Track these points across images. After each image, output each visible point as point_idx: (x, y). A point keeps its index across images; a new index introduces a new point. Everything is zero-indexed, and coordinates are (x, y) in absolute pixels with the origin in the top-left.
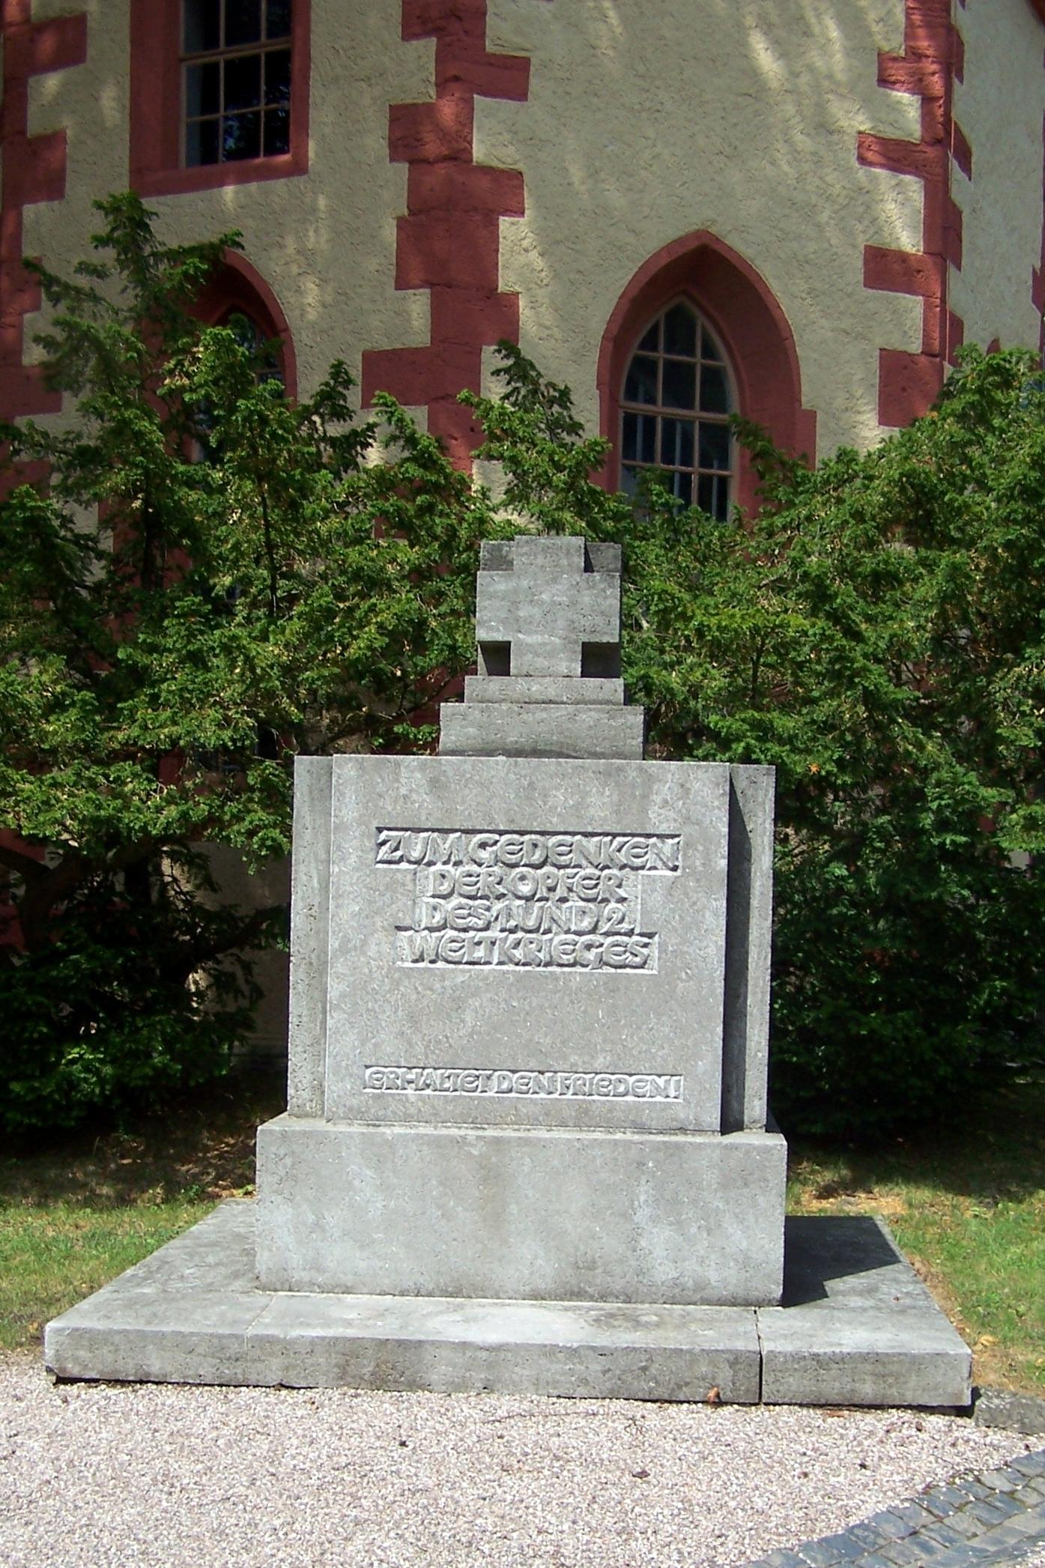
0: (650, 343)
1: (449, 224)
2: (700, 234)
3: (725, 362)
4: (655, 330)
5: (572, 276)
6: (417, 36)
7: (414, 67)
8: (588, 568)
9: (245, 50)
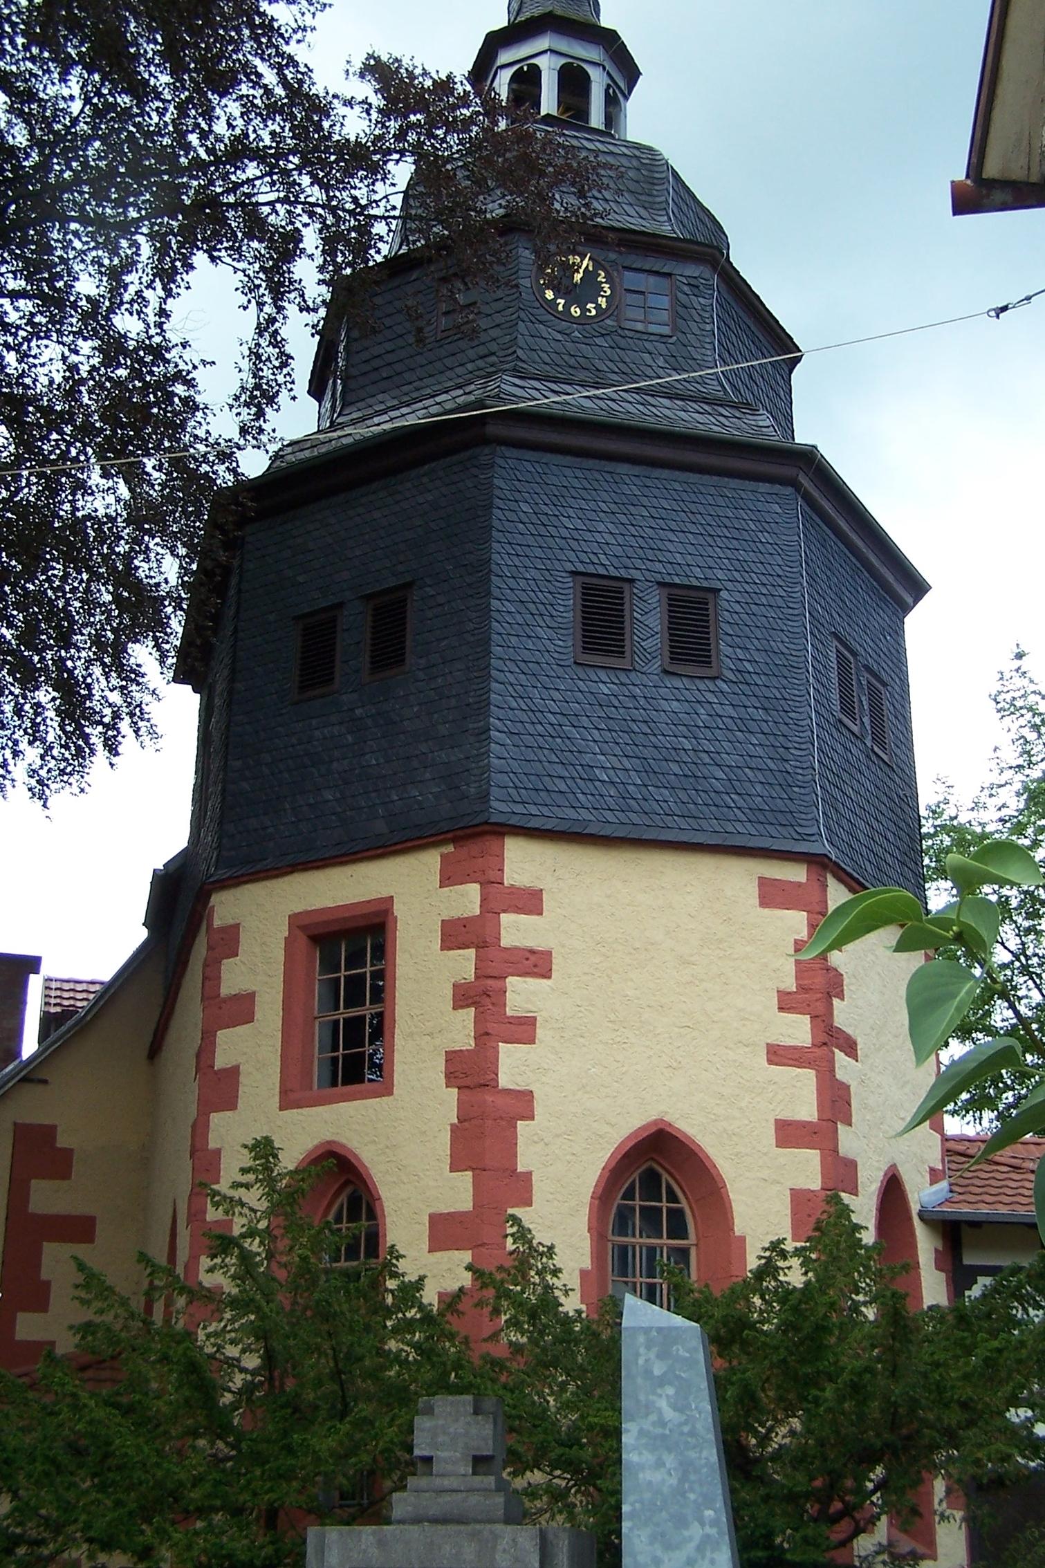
0: (629, 1195)
1: (487, 1123)
2: (655, 1122)
3: (684, 1204)
4: (632, 1186)
5: (568, 1157)
6: (462, 1007)
7: (460, 1030)
8: (476, 1413)
9: (355, 1012)
